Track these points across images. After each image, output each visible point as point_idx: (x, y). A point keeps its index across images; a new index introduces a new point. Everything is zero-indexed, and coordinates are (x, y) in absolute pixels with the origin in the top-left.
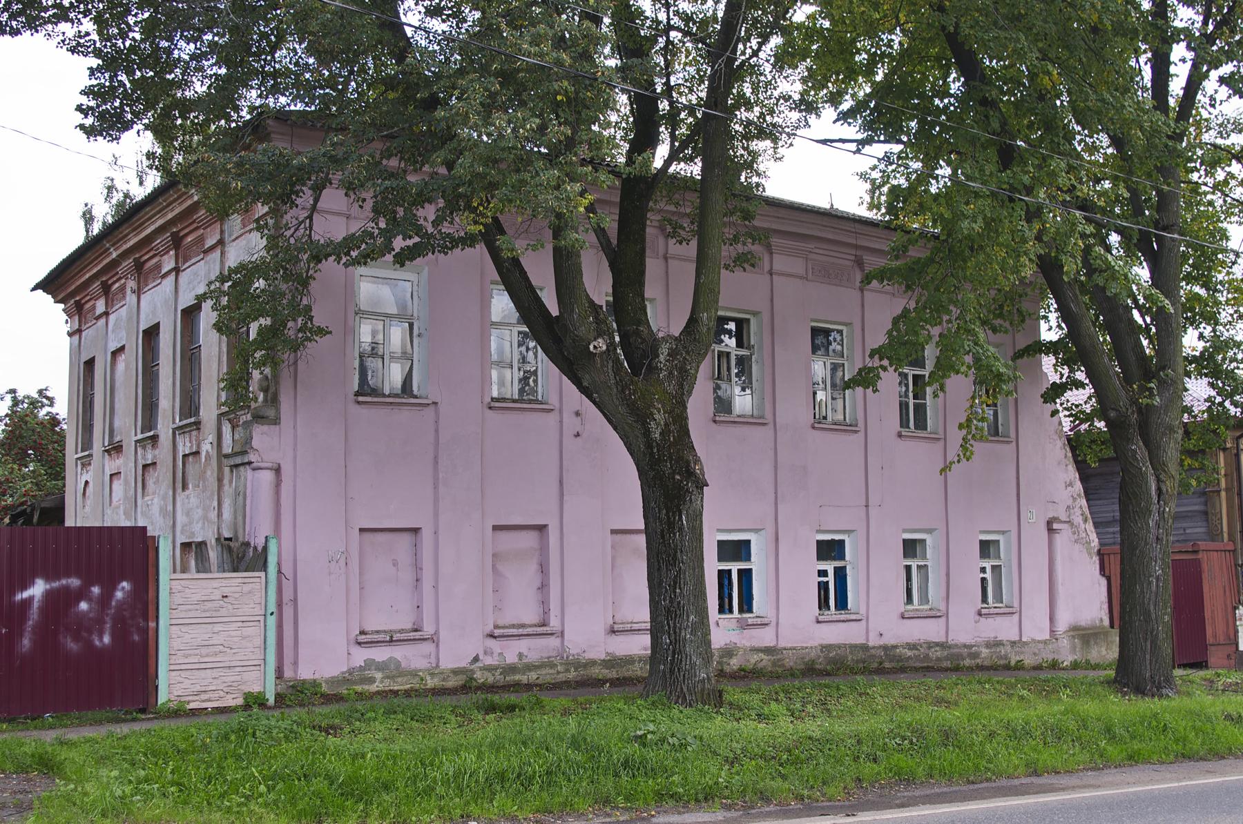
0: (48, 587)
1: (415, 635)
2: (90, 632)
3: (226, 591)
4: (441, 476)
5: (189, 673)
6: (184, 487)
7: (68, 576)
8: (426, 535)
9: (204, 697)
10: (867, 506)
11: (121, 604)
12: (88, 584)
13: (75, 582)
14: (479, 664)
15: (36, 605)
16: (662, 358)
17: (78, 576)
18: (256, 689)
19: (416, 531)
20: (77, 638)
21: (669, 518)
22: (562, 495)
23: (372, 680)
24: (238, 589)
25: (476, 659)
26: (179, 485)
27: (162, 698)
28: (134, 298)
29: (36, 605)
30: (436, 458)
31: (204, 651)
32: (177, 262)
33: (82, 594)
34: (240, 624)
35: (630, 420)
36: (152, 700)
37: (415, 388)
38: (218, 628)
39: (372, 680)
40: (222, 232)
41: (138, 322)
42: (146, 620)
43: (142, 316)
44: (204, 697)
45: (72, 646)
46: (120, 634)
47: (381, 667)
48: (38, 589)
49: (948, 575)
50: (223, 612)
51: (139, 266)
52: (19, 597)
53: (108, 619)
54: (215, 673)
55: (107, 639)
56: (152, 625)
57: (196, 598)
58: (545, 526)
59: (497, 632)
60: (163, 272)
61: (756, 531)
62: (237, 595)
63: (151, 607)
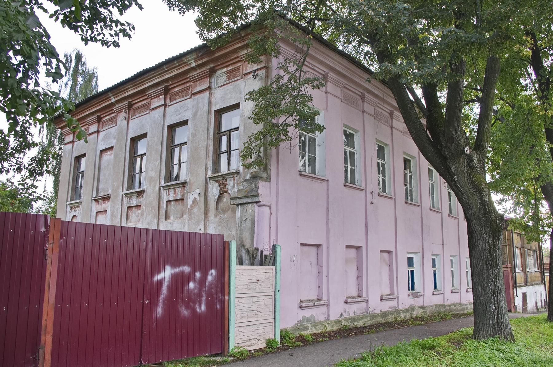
0: (173, 272)
1: (318, 302)
2: (194, 303)
3: (259, 277)
4: (330, 218)
5: (242, 328)
6: (167, 217)
7: (183, 265)
8: (324, 247)
9: (249, 343)
10: (443, 245)
11: (211, 284)
12: (194, 271)
13: (187, 269)
14: (342, 318)
15: (166, 284)
16: (475, 161)
17: (189, 265)
18: (271, 337)
19: (318, 246)
20: (188, 307)
21: (494, 243)
22: (367, 232)
23: (306, 328)
24: (263, 276)
25: (341, 315)
26: (163, 217)
27: (232, 345)
28: (125, 122)
29: (166, 284)
30: (328, 209)
31: (249, 314)
32: (165, 101)
33: (190, 277)
34: (264, 297)
35: (473, 191)
36: (226, 347)
37: (317, 172)
38: (255, 299)
39: (306, 328)
40: (210, 83)
41: (127, 134)
42: (224, 295)
43: (130, 130)
44: (249, 343)
45: (185, 312)
46: (210, 305)
47: (308, 320)
48: (167, 273)
49: (460, 275)
50: (257, 290)
51: (130, 106)
52: (156, 278)
53: (204, 294)
54: (254, 328)
55: (203, 307)
56: (227, 298)
57: (246, 281)
58: (360, 247)
59: (349, 300)
60: (152, 107)
61: (415, 253)
62: (263, 280)
63: (226, 287)
